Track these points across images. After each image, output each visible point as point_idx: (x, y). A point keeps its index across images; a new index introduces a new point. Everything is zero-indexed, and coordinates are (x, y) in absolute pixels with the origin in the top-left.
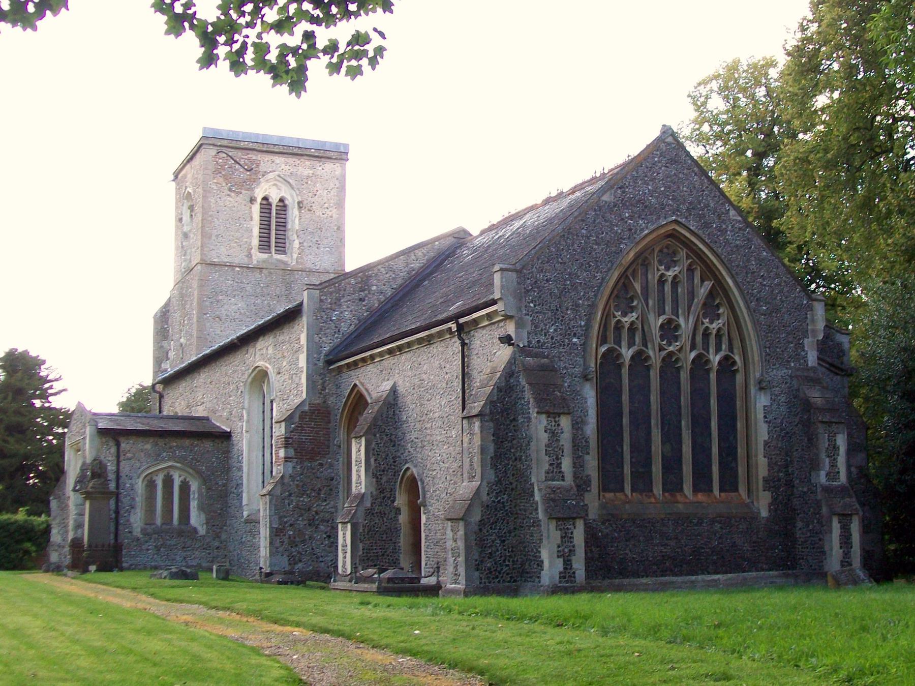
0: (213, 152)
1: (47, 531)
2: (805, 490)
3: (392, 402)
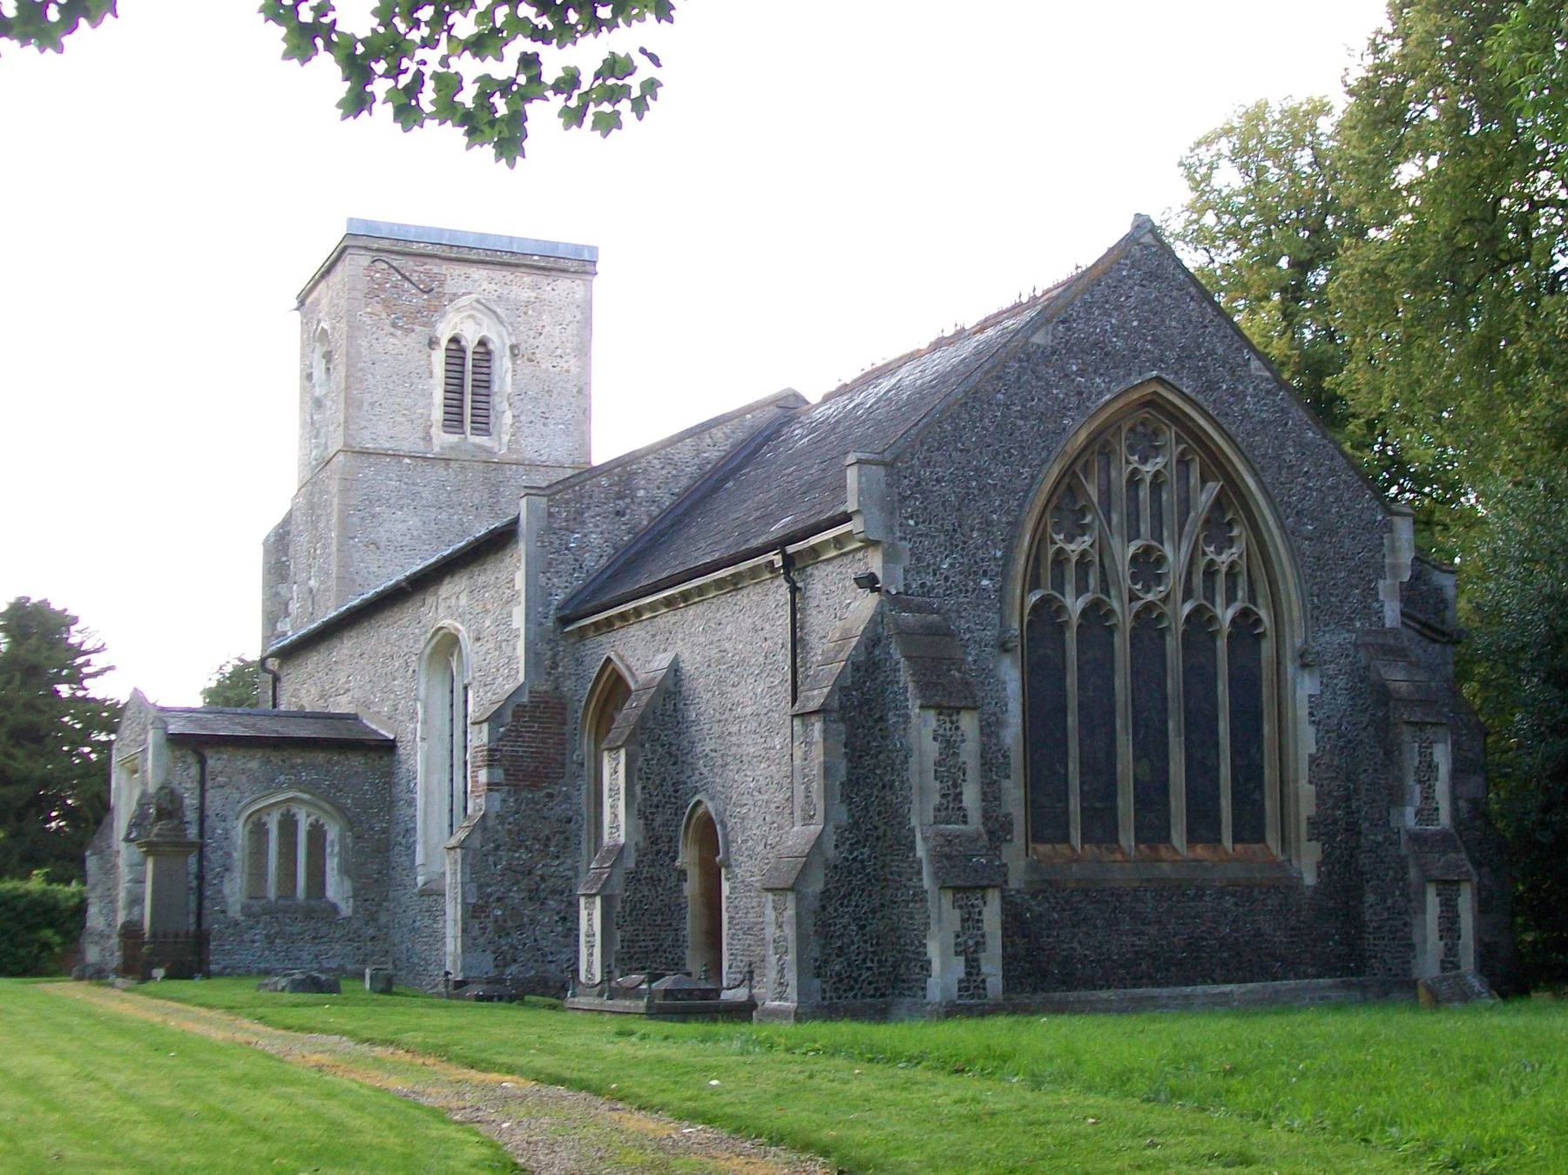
0: (365, 260)
1: (81, 909)
2: (1380, 838)
3: (672, 688)
